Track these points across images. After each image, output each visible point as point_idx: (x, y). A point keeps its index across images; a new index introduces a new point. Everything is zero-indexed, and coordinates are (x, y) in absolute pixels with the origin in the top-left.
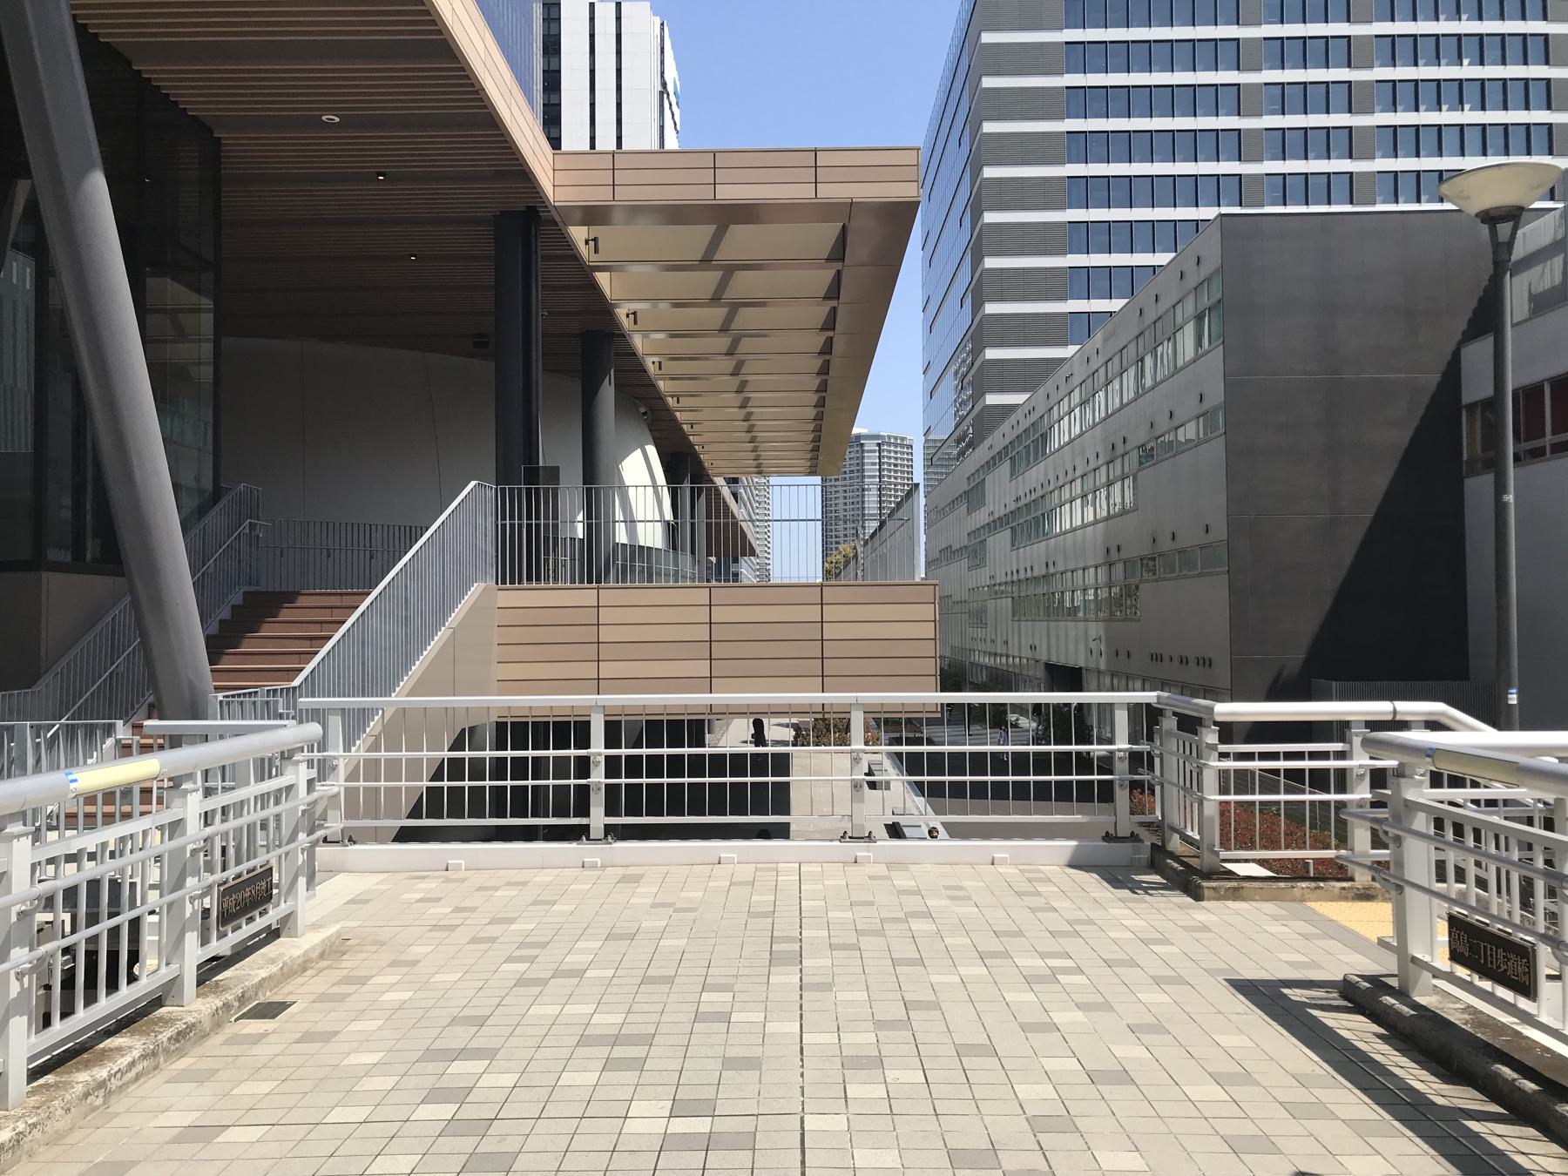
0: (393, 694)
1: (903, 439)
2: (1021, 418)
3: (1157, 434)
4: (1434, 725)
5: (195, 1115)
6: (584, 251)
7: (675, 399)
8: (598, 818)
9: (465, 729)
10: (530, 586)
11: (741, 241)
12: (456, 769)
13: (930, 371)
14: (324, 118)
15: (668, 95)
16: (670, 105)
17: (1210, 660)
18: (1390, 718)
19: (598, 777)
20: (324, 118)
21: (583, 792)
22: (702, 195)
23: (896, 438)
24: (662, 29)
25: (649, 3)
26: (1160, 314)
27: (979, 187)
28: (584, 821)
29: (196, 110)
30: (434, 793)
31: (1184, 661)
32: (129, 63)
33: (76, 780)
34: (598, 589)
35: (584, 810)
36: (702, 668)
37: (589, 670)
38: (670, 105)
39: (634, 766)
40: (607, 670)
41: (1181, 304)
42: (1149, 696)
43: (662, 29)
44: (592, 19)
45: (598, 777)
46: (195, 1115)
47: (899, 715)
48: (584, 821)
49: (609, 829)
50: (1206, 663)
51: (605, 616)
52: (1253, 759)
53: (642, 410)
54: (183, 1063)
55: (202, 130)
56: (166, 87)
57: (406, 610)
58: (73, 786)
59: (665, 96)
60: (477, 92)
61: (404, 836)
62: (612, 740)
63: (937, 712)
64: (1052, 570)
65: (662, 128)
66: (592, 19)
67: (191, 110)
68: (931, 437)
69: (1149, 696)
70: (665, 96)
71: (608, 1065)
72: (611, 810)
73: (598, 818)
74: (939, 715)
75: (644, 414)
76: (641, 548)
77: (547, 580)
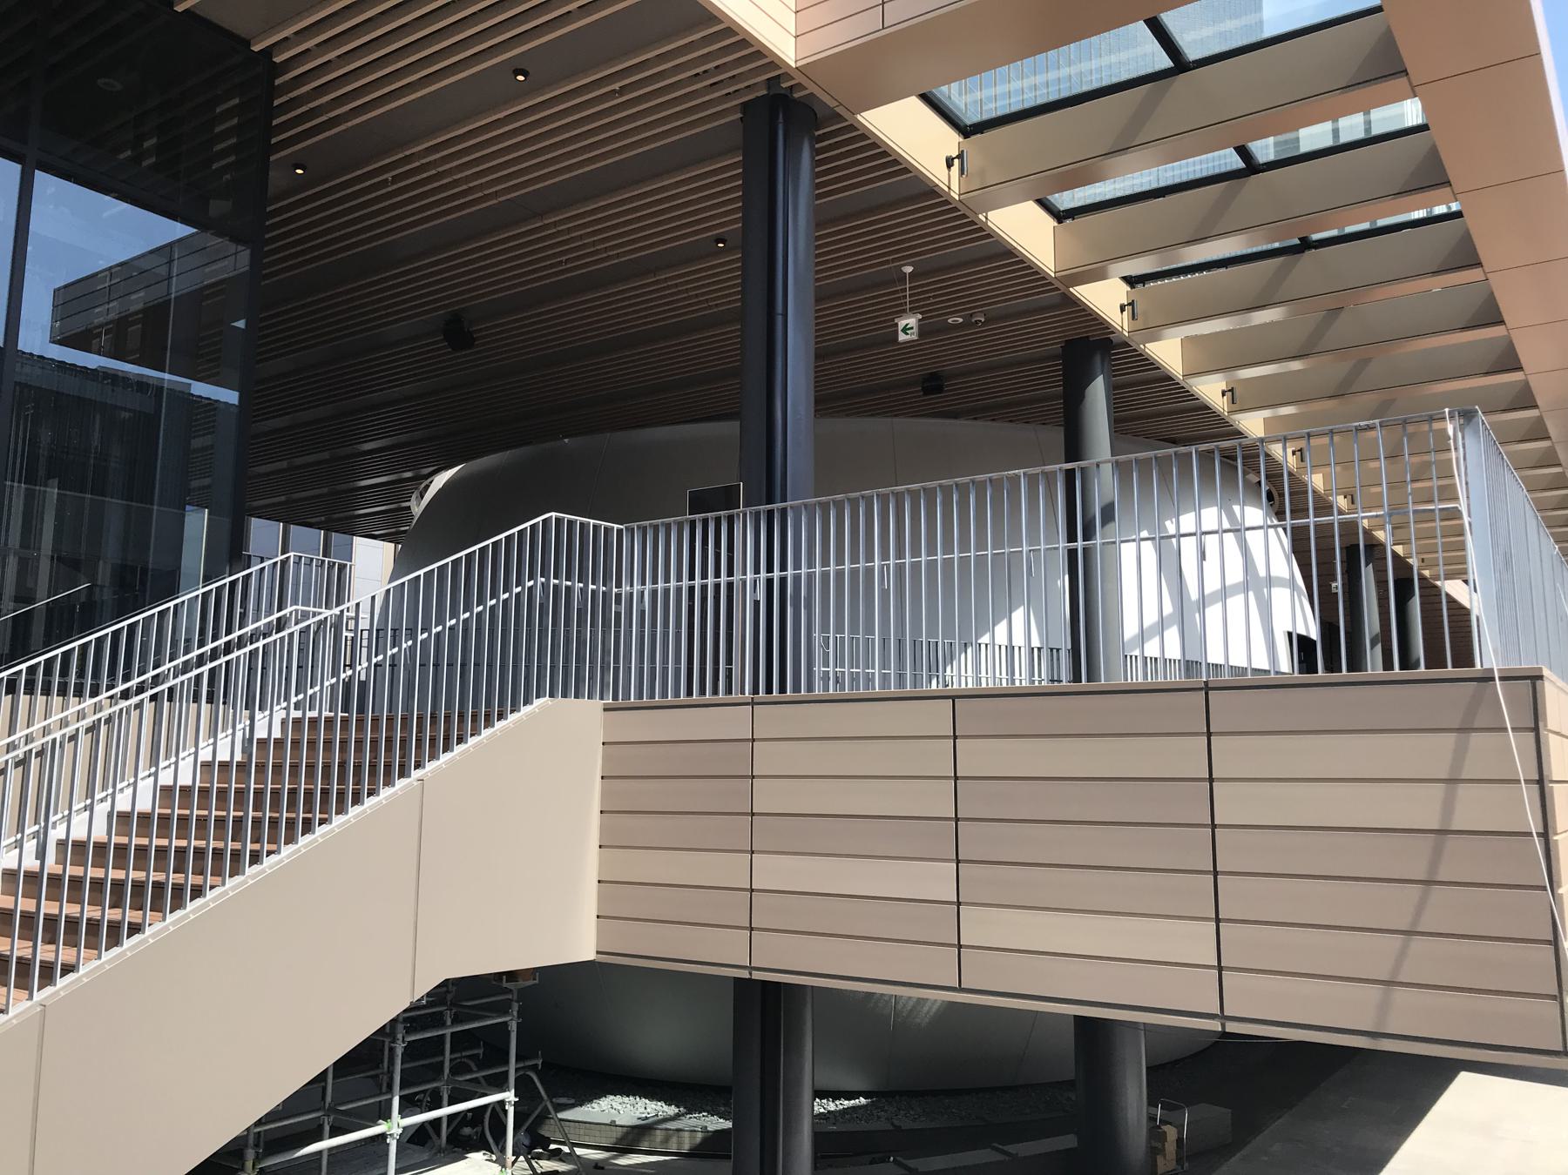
14: (950, 321)
20: (950, 321)
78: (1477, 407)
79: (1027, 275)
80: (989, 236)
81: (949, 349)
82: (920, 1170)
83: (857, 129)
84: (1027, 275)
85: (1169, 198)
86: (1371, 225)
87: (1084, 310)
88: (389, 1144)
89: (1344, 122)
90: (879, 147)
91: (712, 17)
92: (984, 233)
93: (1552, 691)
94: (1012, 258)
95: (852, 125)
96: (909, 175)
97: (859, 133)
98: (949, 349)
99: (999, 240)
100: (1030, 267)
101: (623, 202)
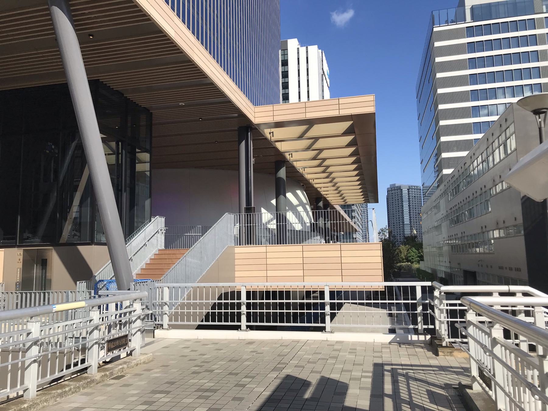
0: (196, 282)
1: (417, 187)
2: (450, 179)
3: (496, 184)
4: (526, 294)
5: (81, 404)
6: (268, 136)
7: (312, 180)
8: (244, 322)
9: (222, 293)
10: (248, 246)
11: (317, 130)
12: (220, 306)
13: (423, 163)
14: (180, 104)
15: (325, 75)
16: (326, 78)
17: (520, 268)
18: (508, 292)
19: (244, 309)
20: (180, 104)
21: (239, 314)
22: (301, 117)
23: (414, 187)
24: (322, 54)
25: (316, 46)
26: (494, 140)
27: (437, 97)
28: (239, 324)
29: (144, 105)
30: (176, 313)
31: (511, 269)
32: (123, 95)
33: (55, 307)
34: (266, 246)
35: (239, 320)
36: (300, 273)
37: (263, 273)
38: (326, 78)
39: (255, 306)
40: (270, 273)
41: (501, 136)
42: (429, 284)
43: (322, 54)
44: (298, 53)
45: (244, 309)
46: (81, 404)
47: (256, 290)
48: (239, 324)
49: (248, 327)
50: (518, 270)
51: (269, 255)
52: (457, 306)
53: (302, 184)
54: (86, 390)
55: (147, 111)
56: (134, 100)
57: (201, 255)
58: (54, 309)
59: (324, 76)
60: (222, 93)
61: (200, 327)
62: (248, 298)
63: (383, 289)
64: (463, 235)
65: (323, 86)
66: (298, 53)
67: (143, 106)
68: (425, 186)
69: (429, 284)
70: (324, 76)
71: (200, 397)
72: (248, 320)
73: (244, 322)
74: (384, 290)
75: (303, 185)
76: (297, 231)
77: (253, 244)
78: (539, 389)
79: (195, 70)
80: (226, 97)
81: (164, 101)
82: (538, 375)
83: (170, 40)
84: (195, 70)
85: (512, 144)
86: (420, 330)
87: (240, 111)
88: (527, 375)
89: (417, 339)
90: (138, 7)
91: (137, 6)
92: (167, 38)
93: (274, 133)
94: (161, 34)
95: (136, 5)
96: (150, 22)
97: (164, 34)
98: (164, 101)
99: (154, 22)
100: (201, 72)
101: (140, 71)
